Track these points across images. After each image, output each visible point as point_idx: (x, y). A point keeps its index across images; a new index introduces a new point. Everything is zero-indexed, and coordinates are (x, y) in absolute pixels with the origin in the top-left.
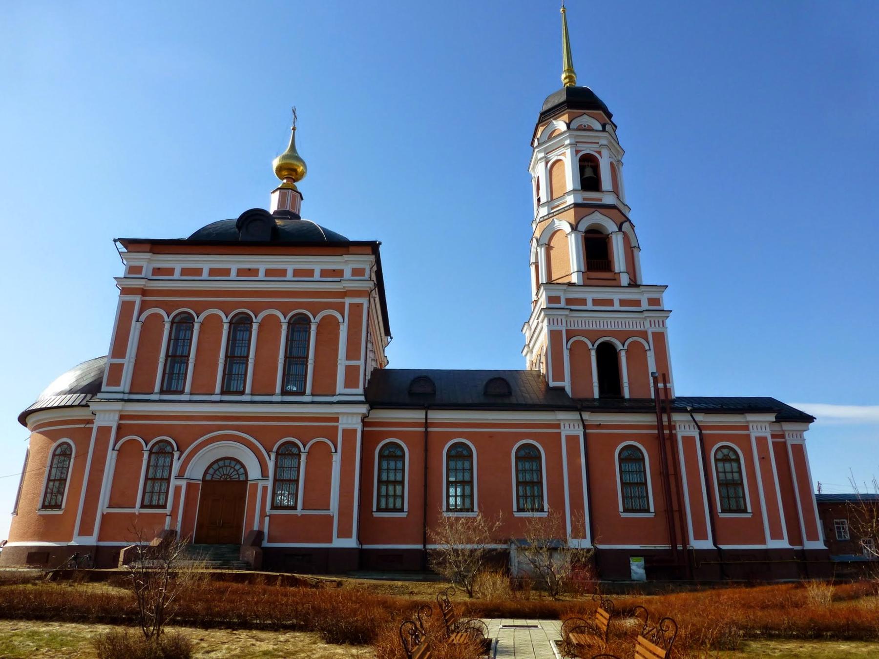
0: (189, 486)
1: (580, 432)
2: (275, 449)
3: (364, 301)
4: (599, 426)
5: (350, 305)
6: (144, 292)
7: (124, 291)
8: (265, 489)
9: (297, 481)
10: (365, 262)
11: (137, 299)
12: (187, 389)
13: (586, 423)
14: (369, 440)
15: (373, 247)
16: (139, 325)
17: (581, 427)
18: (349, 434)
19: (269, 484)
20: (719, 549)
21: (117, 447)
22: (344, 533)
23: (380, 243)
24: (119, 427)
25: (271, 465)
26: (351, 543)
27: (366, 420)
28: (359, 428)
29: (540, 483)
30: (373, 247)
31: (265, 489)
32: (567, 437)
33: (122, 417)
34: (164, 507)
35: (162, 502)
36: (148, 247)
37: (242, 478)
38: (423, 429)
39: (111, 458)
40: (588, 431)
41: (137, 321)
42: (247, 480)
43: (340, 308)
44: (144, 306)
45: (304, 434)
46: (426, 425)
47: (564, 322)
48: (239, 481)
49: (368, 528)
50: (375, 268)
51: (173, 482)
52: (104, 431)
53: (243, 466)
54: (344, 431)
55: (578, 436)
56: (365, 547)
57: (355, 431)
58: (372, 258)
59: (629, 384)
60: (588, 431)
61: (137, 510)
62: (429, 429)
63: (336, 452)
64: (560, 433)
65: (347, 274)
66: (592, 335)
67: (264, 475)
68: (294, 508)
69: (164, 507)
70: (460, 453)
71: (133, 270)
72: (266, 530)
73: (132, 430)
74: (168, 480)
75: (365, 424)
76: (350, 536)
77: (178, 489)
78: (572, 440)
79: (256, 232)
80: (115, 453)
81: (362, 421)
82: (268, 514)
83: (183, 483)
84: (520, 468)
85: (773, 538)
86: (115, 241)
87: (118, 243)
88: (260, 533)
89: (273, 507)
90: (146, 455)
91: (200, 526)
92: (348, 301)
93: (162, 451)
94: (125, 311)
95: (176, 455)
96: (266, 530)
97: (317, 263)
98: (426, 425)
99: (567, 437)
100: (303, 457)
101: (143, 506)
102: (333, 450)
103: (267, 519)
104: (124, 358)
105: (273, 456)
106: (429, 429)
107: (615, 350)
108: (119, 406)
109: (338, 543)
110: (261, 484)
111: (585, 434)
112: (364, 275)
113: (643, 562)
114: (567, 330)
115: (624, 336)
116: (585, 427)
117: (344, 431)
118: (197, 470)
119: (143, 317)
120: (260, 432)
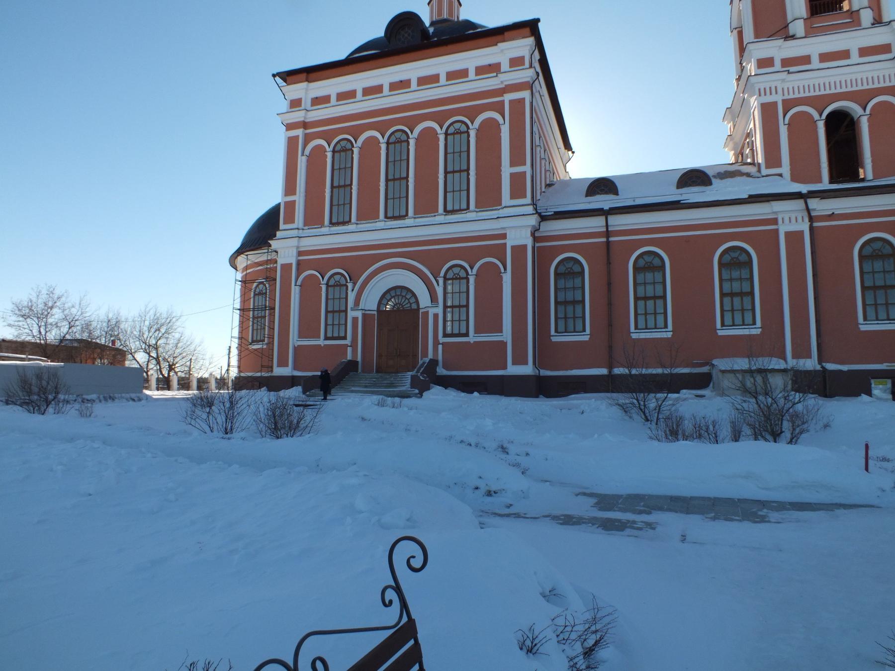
0: (364, 315)
1: (805, 227)
2: (442, 274)
3: (525, 94)
4: (832, 217)
5: (511, 102)
6: (305, 125)
7: (289, 127)
8: (436, 316)
9: (467, 306)
10: (523, 46)
11: (299, 132)
12: (354, 219)
13: (813, 214)
14: (542, 256)
15: (531, 27)
16: (304, 158)
17: (807, 219)
18: (519, 250)
19: (439, 310)
20: (824, 370)
21: (299, 283)
22: (520, 359)
23: (538, 20)
24: (299, 263)
25: (440, 291)
26: (527, 370)
27: (536, 235)
28: (529, 242)
29: (751, 293)
30: (531, 27)
31: (436, 316)
32: (787, 234)
33: (300, 253)
34: (345, 338)
35: (342, 334)
36: (304, 76)
37: (414, 306)
38: (604, 240)
39: (295, 292)
40: (815, 224)
41: (303, 155)
42: (418, 309)
43: (499, 108)
44: (308, 139)
45: (472, 255)
46: (608, 234)
47: (780, 91)
48: (412, 310)
49: (546, 352)
50: (537, 56)
51: (351, 314)
52: (286, 267)
53: (414, 295)
54: (513, 247)
55: (801, 233)
56: (831, 366)
57: (525, 246)
58: (531, 40)
59: (872, 161)
60: (815, 224)
61: (321, 342)
62: (611, 239)
63: (505, 269)
64: (777, 231)
65: (505, 66)
66: (819, 102)
67: (433, 298)
68: (466, 335)
69: (345, 338)
70: (649, 266)
71: (295, 104)
72: (440, 358)
73: (309, 265)
74: (346, 311)
75: (536, 239)
76: (526, 363)
77: (355, 320)
78: (794, 238)
79: (405, 38)
80: (298, 288)
81: (533, 234)
82: (441, 342)
83: (359, 314)
84: (725, 276)
85: (514, 363)
86: (274, 76)
87: (277, 78)
88: (434, 363)
89: (445, 335)
90: (324, 288)
91: (379, 356)
92: (508, 97)
93: (337, 285)
94: (292, 144)
95: (350, 285)
96: (440, 358)
97: (469, 59)
98: (608, 234)
99: (787, 234)
100: (472, 280)
101: (326, 338)
102: (503, 270)
103: (440, 347)
104: (295, 194)
105: (441, 281)
106: (611, 239)
107: (852, 119)
108: (294, 242)
109: (513, 370)
110: (432, 311)
111: (812, 228)
112: (524, 64)
113: (889, 385)
114: (784, 101)
115: (862, 97)
116: (811, 219)
117: (513, 247)
118: (370, 302)
119: (307, 152)
120: (431, 258)
